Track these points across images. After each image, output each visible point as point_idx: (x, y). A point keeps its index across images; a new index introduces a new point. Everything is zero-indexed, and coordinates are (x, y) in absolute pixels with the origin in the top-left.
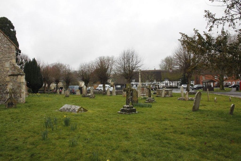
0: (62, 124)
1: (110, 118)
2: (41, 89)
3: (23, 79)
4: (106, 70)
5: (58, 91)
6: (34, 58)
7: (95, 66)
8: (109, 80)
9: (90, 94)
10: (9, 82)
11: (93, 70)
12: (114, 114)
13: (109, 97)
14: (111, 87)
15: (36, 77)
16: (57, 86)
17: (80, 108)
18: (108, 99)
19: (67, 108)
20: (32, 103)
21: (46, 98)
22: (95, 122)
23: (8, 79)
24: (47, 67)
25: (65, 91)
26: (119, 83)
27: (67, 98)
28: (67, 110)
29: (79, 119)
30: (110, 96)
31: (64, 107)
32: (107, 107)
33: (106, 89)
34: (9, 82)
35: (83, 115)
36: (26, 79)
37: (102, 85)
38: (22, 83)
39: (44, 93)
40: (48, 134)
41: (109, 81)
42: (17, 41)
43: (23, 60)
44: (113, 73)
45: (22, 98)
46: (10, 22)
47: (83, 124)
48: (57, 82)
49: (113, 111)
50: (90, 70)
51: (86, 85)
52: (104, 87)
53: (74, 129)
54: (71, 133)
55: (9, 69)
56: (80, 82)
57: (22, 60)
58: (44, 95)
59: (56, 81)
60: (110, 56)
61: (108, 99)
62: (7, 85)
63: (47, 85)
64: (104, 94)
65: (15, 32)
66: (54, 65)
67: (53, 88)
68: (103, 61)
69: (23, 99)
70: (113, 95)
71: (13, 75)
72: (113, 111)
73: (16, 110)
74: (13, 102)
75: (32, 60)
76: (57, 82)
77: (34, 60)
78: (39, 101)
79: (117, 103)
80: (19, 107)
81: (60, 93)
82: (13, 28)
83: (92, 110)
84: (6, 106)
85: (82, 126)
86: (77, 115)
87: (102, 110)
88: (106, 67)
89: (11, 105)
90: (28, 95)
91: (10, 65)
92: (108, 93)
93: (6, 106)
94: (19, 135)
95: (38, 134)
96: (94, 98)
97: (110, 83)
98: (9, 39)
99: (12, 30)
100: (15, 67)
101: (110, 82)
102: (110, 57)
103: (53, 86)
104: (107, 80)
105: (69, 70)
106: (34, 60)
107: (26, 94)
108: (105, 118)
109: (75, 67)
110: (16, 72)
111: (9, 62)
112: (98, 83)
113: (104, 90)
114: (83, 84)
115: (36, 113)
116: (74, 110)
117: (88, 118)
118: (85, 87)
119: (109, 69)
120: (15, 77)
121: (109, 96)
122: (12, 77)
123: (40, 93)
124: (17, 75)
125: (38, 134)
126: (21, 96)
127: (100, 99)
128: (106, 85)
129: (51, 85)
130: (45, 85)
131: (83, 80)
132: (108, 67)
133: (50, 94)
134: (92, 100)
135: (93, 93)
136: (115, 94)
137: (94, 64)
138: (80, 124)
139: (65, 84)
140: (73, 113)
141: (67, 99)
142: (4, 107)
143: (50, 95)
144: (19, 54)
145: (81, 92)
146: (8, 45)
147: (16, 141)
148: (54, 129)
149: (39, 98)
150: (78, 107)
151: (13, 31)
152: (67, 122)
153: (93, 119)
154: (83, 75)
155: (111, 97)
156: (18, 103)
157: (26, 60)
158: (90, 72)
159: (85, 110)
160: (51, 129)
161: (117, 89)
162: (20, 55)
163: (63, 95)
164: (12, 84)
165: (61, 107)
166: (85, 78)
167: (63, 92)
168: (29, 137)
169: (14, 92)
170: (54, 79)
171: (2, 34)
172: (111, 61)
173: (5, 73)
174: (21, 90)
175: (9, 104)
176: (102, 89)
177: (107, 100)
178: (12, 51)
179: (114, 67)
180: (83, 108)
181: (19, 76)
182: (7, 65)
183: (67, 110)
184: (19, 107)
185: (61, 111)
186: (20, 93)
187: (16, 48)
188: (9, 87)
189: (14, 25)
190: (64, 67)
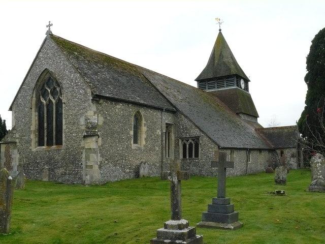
77: (196, 80)
98: (42, 77)
106: (196, 80)
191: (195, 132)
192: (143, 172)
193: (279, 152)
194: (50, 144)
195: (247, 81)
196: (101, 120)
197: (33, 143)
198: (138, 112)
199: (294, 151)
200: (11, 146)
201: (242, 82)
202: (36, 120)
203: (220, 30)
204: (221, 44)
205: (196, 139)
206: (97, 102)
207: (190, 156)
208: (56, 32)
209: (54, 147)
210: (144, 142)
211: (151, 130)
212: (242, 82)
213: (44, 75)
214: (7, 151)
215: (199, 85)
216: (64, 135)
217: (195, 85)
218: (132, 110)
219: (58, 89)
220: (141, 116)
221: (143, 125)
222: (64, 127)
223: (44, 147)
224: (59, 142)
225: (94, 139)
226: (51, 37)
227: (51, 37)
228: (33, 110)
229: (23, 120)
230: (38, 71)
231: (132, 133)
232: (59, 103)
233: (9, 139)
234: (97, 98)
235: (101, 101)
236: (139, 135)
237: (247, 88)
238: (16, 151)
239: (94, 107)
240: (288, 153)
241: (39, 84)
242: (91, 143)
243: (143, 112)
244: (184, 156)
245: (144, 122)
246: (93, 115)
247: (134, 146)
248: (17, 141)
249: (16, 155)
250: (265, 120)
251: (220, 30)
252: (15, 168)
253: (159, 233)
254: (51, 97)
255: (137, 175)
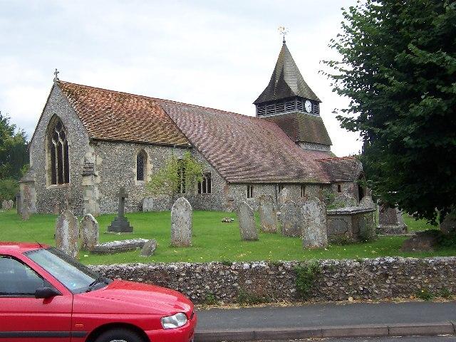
77: (255, 103)
106: (255, 103)
191: (208, 168)
192: (145, 206)
193: (336, 186)
194: (61, 182)
195: (316, 103)
196: (100, 160)
197: (48, 184)
198: (143, 151)
199: (351, 185)
201: (308, 105)
203: (284, 42)
204: (285, 54)
205: (208, 175)
206: (96, 145)
207: (205, 192)
208: (63, 78)
210: (149, 179)
211: (159, 163)
212: (308, 105)
214: (26, 188)
215: (259, 113)
217: (251, 111)
218: (135, 150)
219: (65, 133)
220: (146, 154)
221: (148, 162)
222: (70, 167)
225: (90, 177)
226: (59, 85)
227: (59, 85)
230: (49, 115)
231: (135, 171)
232: (66, 147)
233: (28, 179)
234: (94, 142)
235: (99, 144)
237: (316, 110)
239: (92, 149)
240: (344, 188)
242: (87, 181)
243: (147, 150)
244: (199, 192)
245: (149, 159)
246: (91, 156)
247: (138, 183)
248: (35, 180)
249: (34, 194)
250: (332, 149)
251: (284, 42)
252: (34, 205)
254: (60, 140)
255: (141, 208)
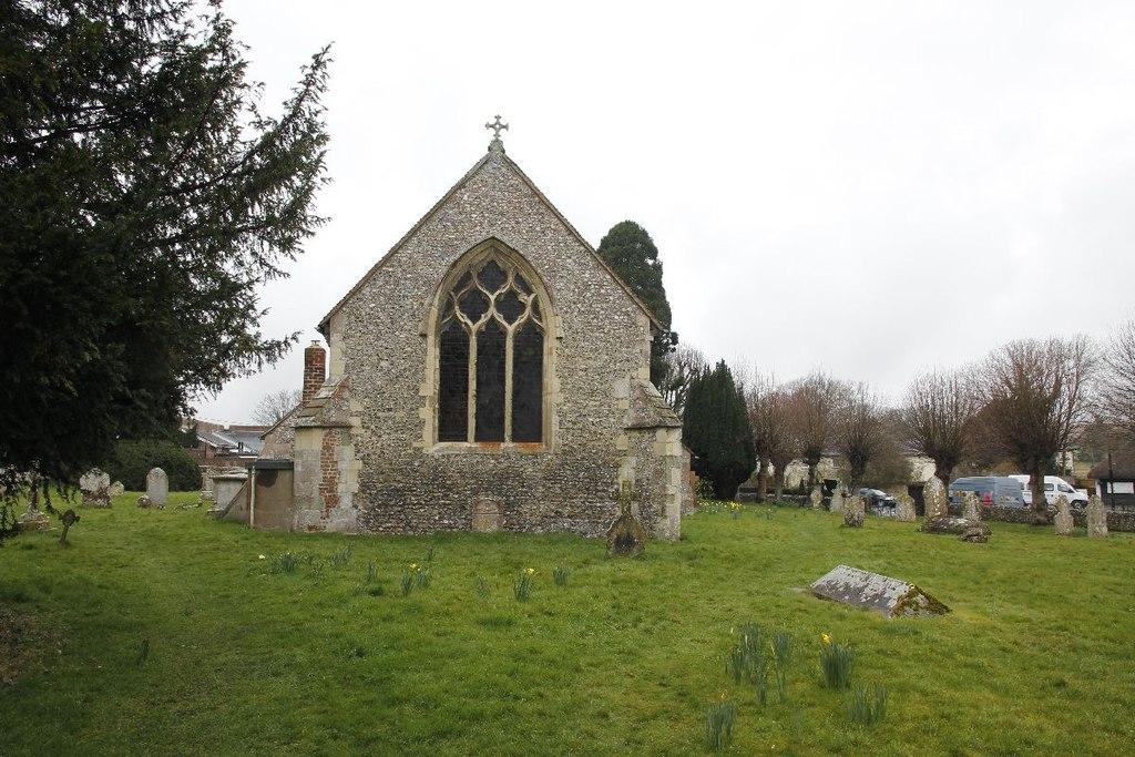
0: (812, 674)
1: (1091, 676)
2: (749, 484)
3: (672, 444)
4: (1046, 404)
5: (816, 495)
6: (723, 361)
7: (987, 388)
8: (1060, 454)
9: (961, 521)
10: (625, 453)
11: (979, 407)
12: (1112, 655)
13: (1066, 542)
14: (1075, 487)
15: (731, 438)
16: (811, 473)
17: (911, 595)
18: (1064, 552)
19: (847, 586)
20: (705, 545)
21: (763, 525)
22: (994, 689)
23: (622, 442)
24: (773, 398)
25: (844, 495)
26: (1124, 471)
27: (853, 531)
28: (844, 593)
29: (904, 652)
30: (1073, 535)
31: (830, 576)
32: (1062, 600)
33: (1051, 497)
34: (625, 453)
35: (925, 634)
36: (687, 441)
37: (1025, 479)
38: (668, 460)
39: (759, 500)
40: (740, 720)
41: (1064, 459)
42: (667, 298)
43: (686, 371)
44: (1084, 417)
45: (668, 522)
46: (644, 233)
47: (924, 693)
48: (812, 456)
49: (1105, 631)
50: (960, 406)
51: (944, 473)
52: (1038, 487)
53: (869, 718)
54: (851, 736)
55: (624, 405)
56: (913, 460)
57: (682, 368)
58: (757, 509)
59: (805, 454)
60: (1067, 336)
61: (1064, 552)
62: (617, 466)
63: (771, 469)
64: (1039, 523)
65: (658, 268)
66: (949, 398)
67: (795, 483)
68: (1029, 360)
69: (672, 522)
70: (1090, 535)
71: (639, 428)
72: (1105, 631)
73: (640, 570)
74: (634, 533)
75: (713, 368)
76: (812, 456)
77: (722, 366)
78: (733, 536)
79: (1118, 579)
80: (655, 556)
81: (826, 504)
82: (653, 252)
83: (976, 607)
84: (609, 548)
85: (913, 707)
86: (890, 631)
87: (1034, 614)
88: (1048, 392)
89: (624, 544)
90: (696, 505)
91: (632, 387)
92: (1064, 521)
93: (609, 548)
94: (616, 696)
95: (696, 706)
96: (982, 539)
97: (1069, 471)
98: (470, 256)
99: (650, 262)
100: (647, 398)
101: (1069, 464)
102: (1066, 342)
103: (796, 473)
104: (1051, 456)
105: (865, 408)
106: (722, 366)
107: (684, 505)
108: (1056, 674)
109: (889, 389)
110: (651, 417)
111: (628, 377)
112: (1004, 465)
113: (1040, 505)
114: (926, 470)
115: (712, 593)
116: (879, 599)
117: (950, 655)
118: (937, 485)
119: (1065, 398)
120: (647, 436)
121: (1069, 535)
122: (636, 434)
123: (745, 500)
124: (653, 429)
125: (696, 706)
126: (663, 510)
127: (1012, 546)
128: (1048, 479)
129: (789, 469)
130: (764, 467)
131: (930, 451)
132: (1057, 392)
133: (780, 506)
134: (974, 553)
135: (981, 514)
136: (1105, 530)
137: (980, 378)
138: (903, 690)
139: (847, 467)
140: (875, 615)
141: (852, 535)
142: (603, 552)
143: (781, 512)
144: (672, 346)
145: (920, 508)
146: (627, 314)
147: (604, 722)
148: (772, 695)
149: (738, 522)
150: (898, 589)
151: (654, 266)
152: (836, 672)
153: (978, 667)
154: (926, 427)
155: (1079, 543)
156: (652, 538)
157: (696, 371)
158: (962, 414)
159: (937, 607)
160: (753, 696)
161: (1111, 500)
162: (674, 350)
163: (836, 514)
164: (633, 461)
165: (823, 574)
166: (937, 440)
167: (836, 501)
168: (655, 717)
169: (645, 494)
170: (798, 444)
171: (608, 277)
172: (1071, 363)
173: (612, 420)
174: (664, 488)
175: (618, 542)
176: (1028, 497)
177: (1058, 559)
178: (637, 336)
179: (1088, 391)
180: (927, 597)
181: (661, 433)
182: (621, 389)
183: (844, 593)
184: (655, 556)
185: (820, 597)
186: (664, 496)
187: (651, 321)
188: (627, 473)
189: (656, 244)
190: (845, 393)
200: (338, 435)
202: (434, 428)
209: (470, 444)
213: (479, 250)
216: (450, 443)
223: (465, 444)
224: (530, 427)
228: (431, 339)
229: (383, 364)
232: (532, 339)
236: (268, 467)
238: (349, 451)
241: (455, 271)
248: (356, 421)
252: (346, 502)
253: (110, 324)
